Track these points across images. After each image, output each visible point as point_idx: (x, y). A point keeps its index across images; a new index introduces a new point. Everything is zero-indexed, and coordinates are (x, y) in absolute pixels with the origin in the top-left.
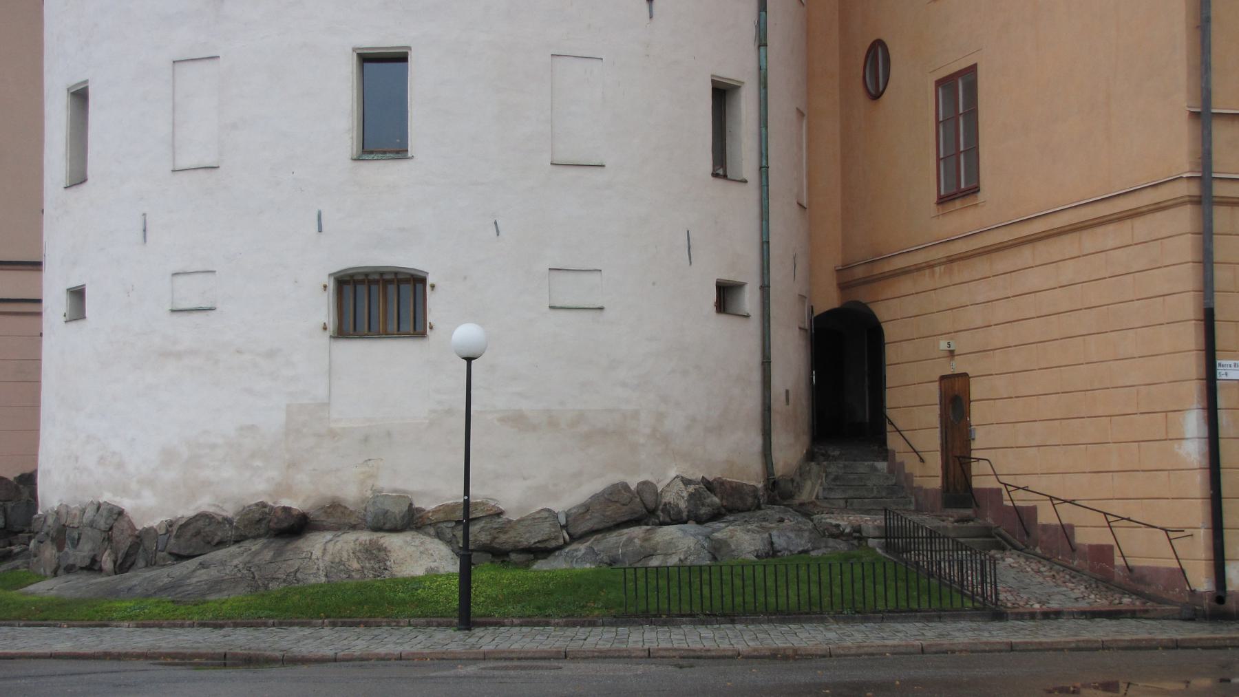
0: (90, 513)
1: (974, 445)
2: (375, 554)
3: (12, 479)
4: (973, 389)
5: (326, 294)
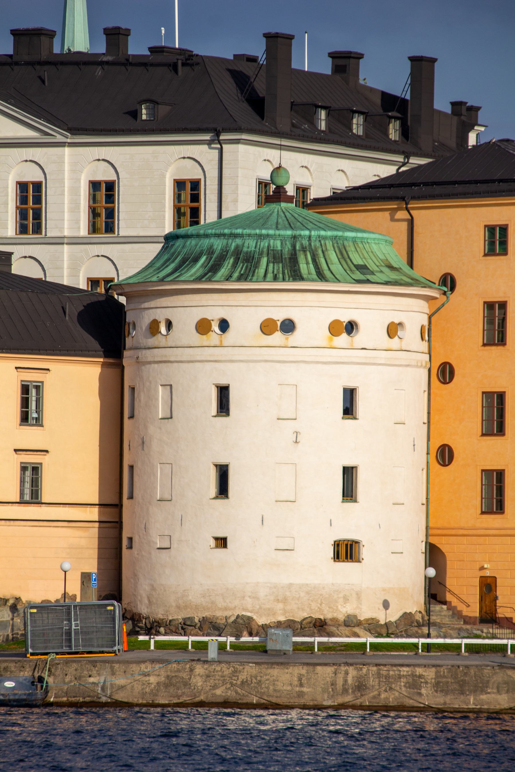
0: (233, 619)
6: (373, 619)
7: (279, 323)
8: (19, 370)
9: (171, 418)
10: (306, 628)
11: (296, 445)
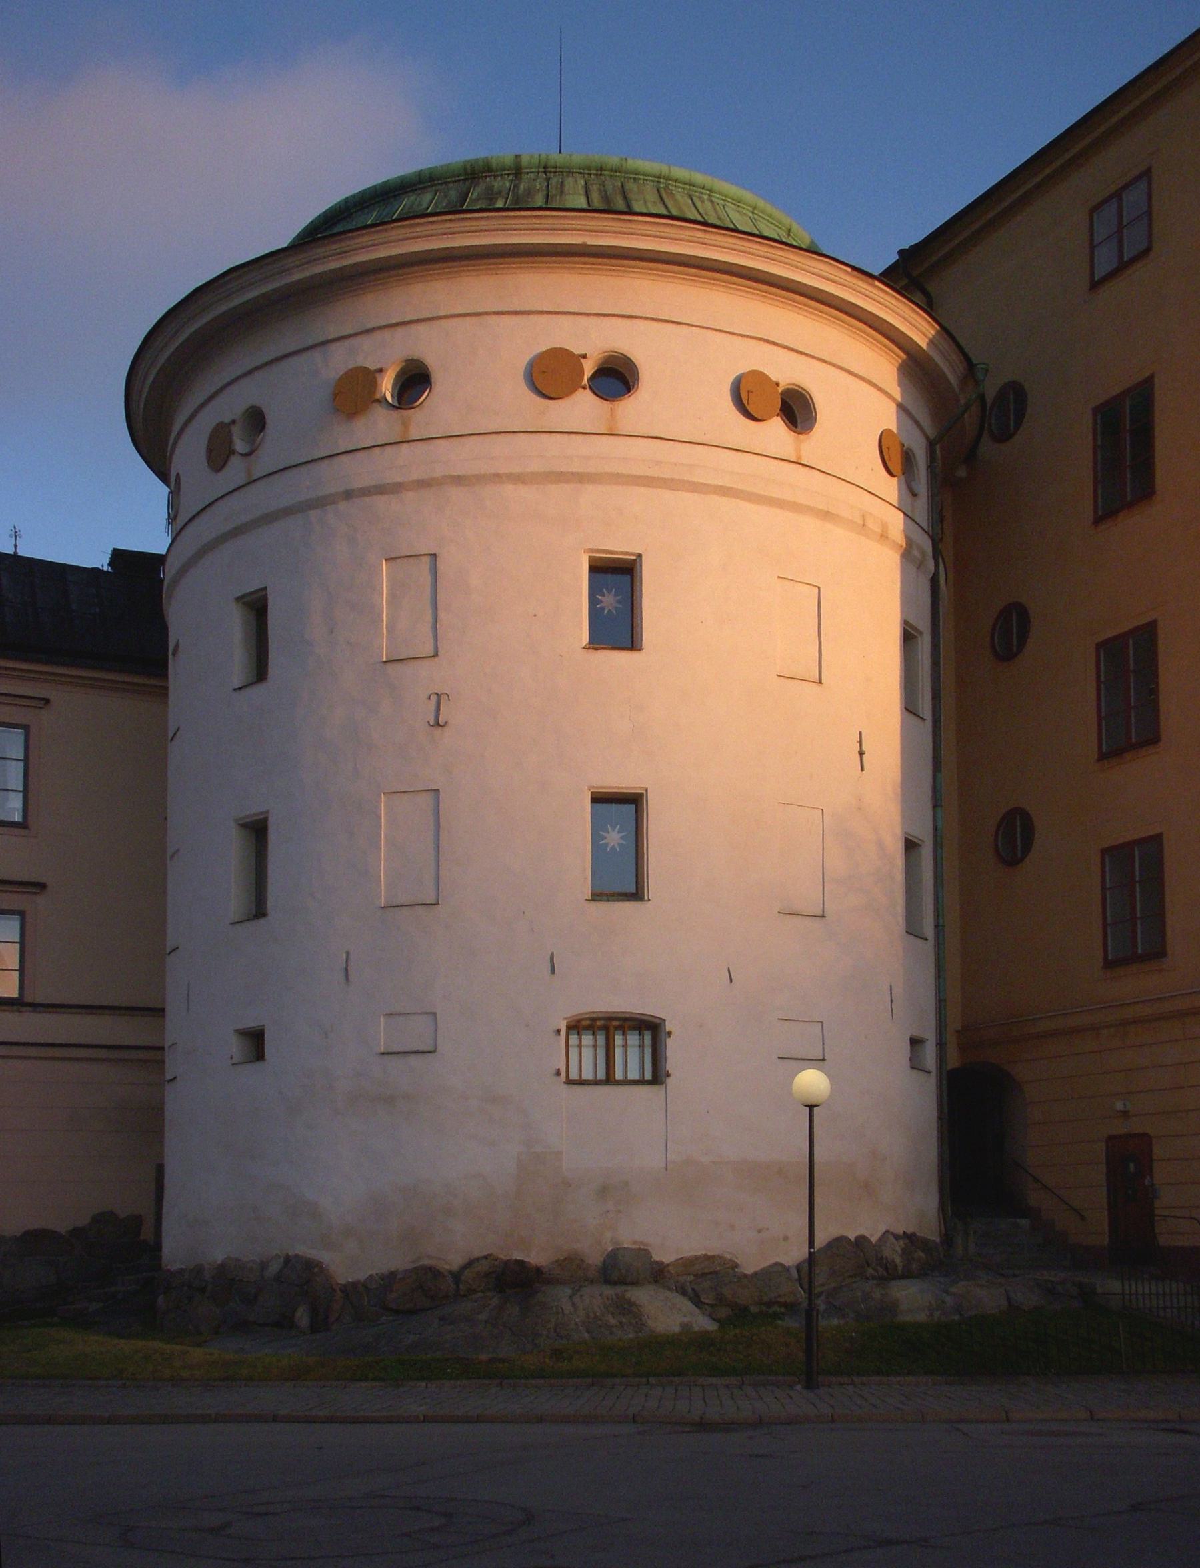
0: (274, 1268)
1: (1157, 1203)
2: (626, 1308)
3: (63, 1232)
5: (668, 1029)
6: (707, 1258)
7: (589, 368)
9: (436, 655)
10: (475, 1291)
11: (438, 731)
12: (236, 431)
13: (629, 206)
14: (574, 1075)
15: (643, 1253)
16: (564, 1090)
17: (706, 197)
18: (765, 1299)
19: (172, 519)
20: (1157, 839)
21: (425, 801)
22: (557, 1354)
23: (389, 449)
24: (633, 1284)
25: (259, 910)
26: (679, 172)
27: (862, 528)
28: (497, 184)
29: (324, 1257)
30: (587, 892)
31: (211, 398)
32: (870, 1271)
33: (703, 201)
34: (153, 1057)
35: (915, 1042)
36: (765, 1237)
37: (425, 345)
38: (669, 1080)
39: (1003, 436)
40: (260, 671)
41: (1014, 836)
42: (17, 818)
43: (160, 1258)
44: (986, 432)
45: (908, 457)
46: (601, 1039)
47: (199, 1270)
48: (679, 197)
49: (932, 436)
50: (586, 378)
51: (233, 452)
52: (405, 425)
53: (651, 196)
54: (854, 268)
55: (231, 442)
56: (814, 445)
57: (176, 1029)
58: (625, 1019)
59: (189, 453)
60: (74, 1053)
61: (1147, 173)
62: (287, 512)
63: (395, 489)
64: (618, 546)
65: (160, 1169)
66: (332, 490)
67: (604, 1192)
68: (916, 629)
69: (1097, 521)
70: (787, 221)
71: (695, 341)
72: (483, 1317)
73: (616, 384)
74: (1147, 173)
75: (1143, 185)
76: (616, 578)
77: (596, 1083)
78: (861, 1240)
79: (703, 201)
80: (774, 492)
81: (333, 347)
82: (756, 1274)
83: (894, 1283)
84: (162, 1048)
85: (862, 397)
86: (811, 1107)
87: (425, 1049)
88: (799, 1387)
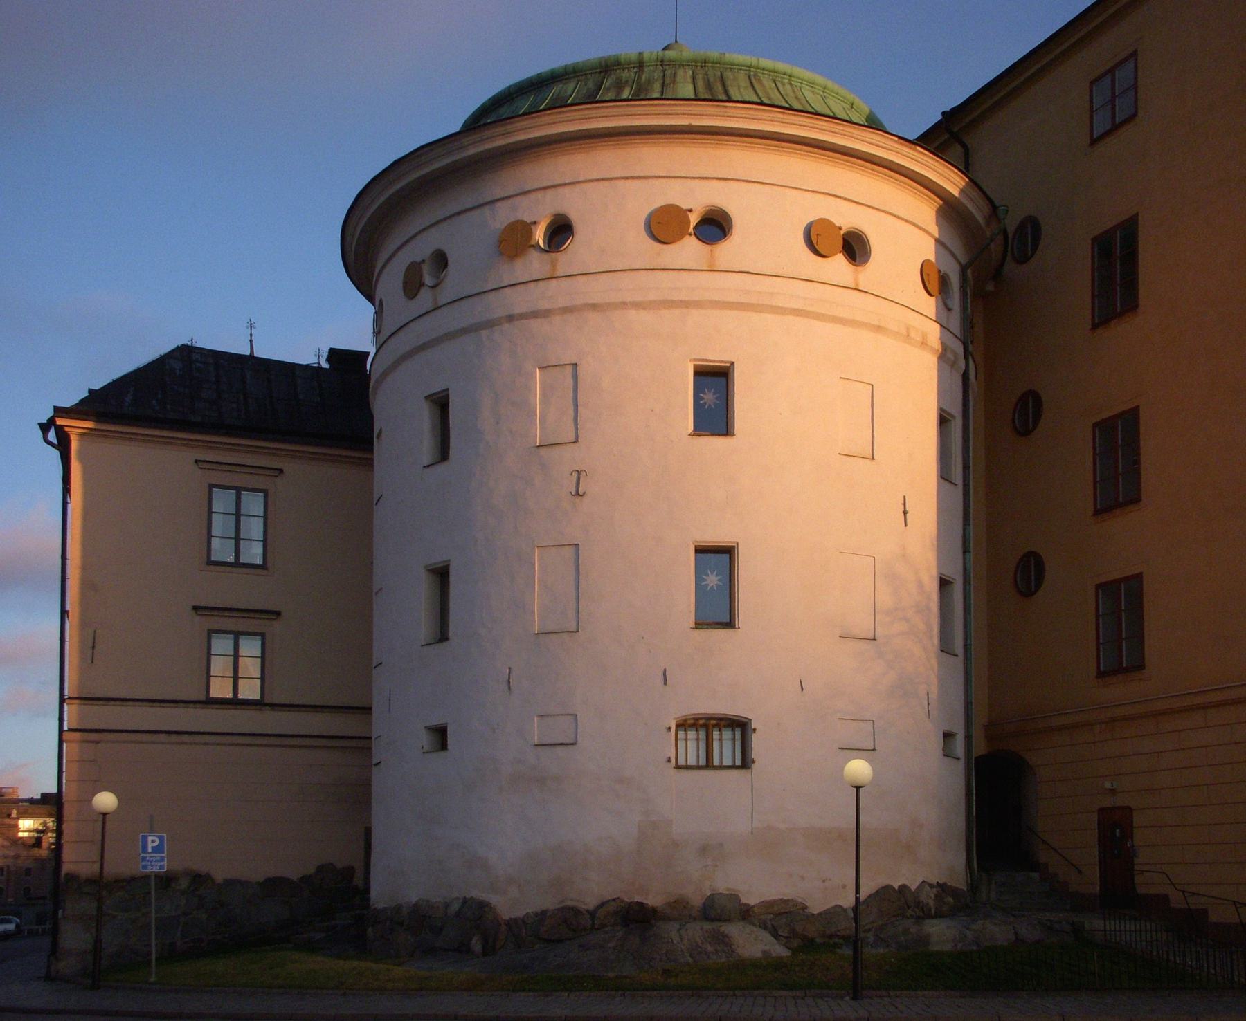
0: (456, 907)
1: (1136, 860)
2: (722, 940)
4: (1135, 819)
6: (786, 902)
7: (694, 219)
8: (201, 465)
9: (576, 441)
11: (578, 500)
12: (426, 269)
13: (726, 92)
14: (682, 762)
15: (734, 897)
16: (673, 772)
17: (786, 81)
18: (828, 932)
19: (376, 333)
20: (1139, 577)
21: (569, 552)
22: (666, 972)
23: (541, 283)
24: (725, 921)
25: (443, 636)
26: (766, 63)
27: (907, 338)
28: (625, 75)
29: (494, 899)
30: (691, 621)
31: (407, 242)
32: (909, 912)
33: (783, 85)
34: (362, 745)
35: (947, 736)
36: (825, 886)
37: (571, 204)
38: (754, 766)
39: (1023, 259)
40: (443, 453)
41: (1030, 574)
42: (259, 561)
43: (368, 899)
44: (1009, 258)
45: (944, 281)
46: (702, 734)
47: (398, 908)
48: (765, 82)
49: (963, 261)
50: (692, 226)
51: (422, 285)
52: (554, 264)
53: (744, 83)
54: (900, 138)
55: (421, 276)
56: (870, 274)
57: (380, 725)
58: (721, 719)
59: (390, 282)
60: (307, 742)
61: (1134, 55)
62: (464, 331)
63: (546, 314)
64: (716, 356)
65: (368, 832)
66: (496, 316)
67: (704, 850)
68: (949, 414)
69: (1095, 327)
70: (851, 97)
71: (774, 194)
72: (611, 945)
73: (717, 231)
74: (1134, 55)
75: (1131, 65)
76: (714, 382)
77: (698, 768)
78: (903, 888)
79: (783, 85)
80: (839, 313)
81: (499, 204)
82: (820, 914)
83: (927, 921)
84: (370, 738)
85: (907, 231)
86: (858, 788)
87: (568, 741)
88: (847, 998)
